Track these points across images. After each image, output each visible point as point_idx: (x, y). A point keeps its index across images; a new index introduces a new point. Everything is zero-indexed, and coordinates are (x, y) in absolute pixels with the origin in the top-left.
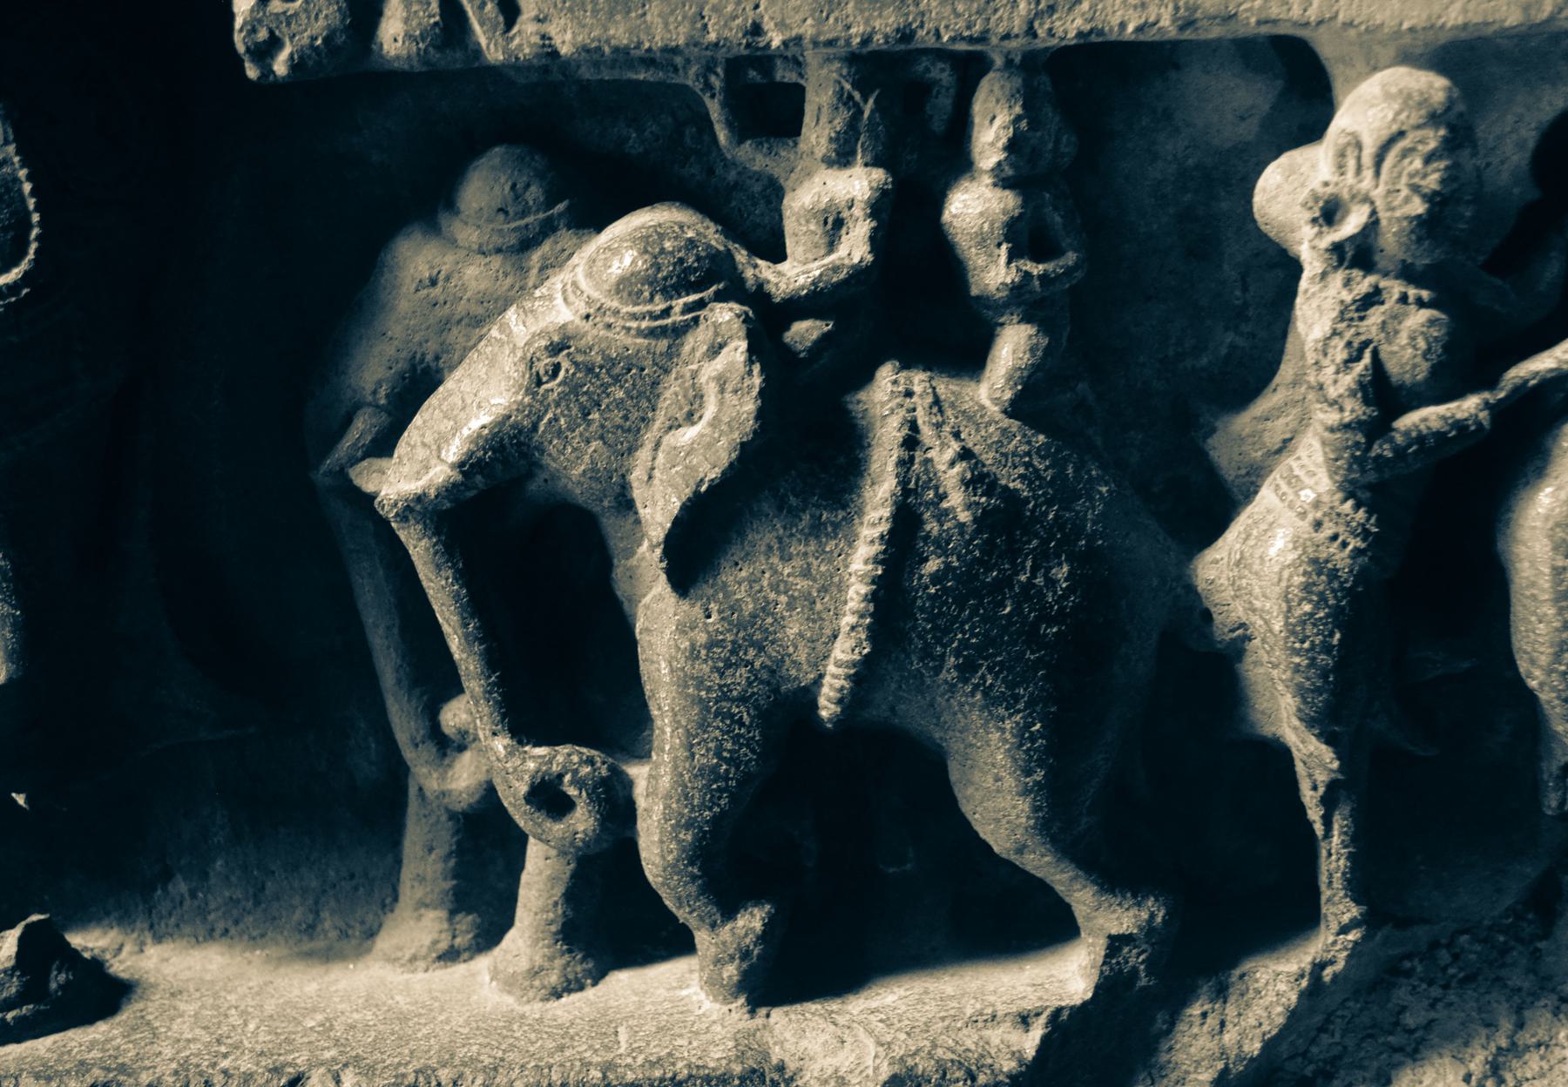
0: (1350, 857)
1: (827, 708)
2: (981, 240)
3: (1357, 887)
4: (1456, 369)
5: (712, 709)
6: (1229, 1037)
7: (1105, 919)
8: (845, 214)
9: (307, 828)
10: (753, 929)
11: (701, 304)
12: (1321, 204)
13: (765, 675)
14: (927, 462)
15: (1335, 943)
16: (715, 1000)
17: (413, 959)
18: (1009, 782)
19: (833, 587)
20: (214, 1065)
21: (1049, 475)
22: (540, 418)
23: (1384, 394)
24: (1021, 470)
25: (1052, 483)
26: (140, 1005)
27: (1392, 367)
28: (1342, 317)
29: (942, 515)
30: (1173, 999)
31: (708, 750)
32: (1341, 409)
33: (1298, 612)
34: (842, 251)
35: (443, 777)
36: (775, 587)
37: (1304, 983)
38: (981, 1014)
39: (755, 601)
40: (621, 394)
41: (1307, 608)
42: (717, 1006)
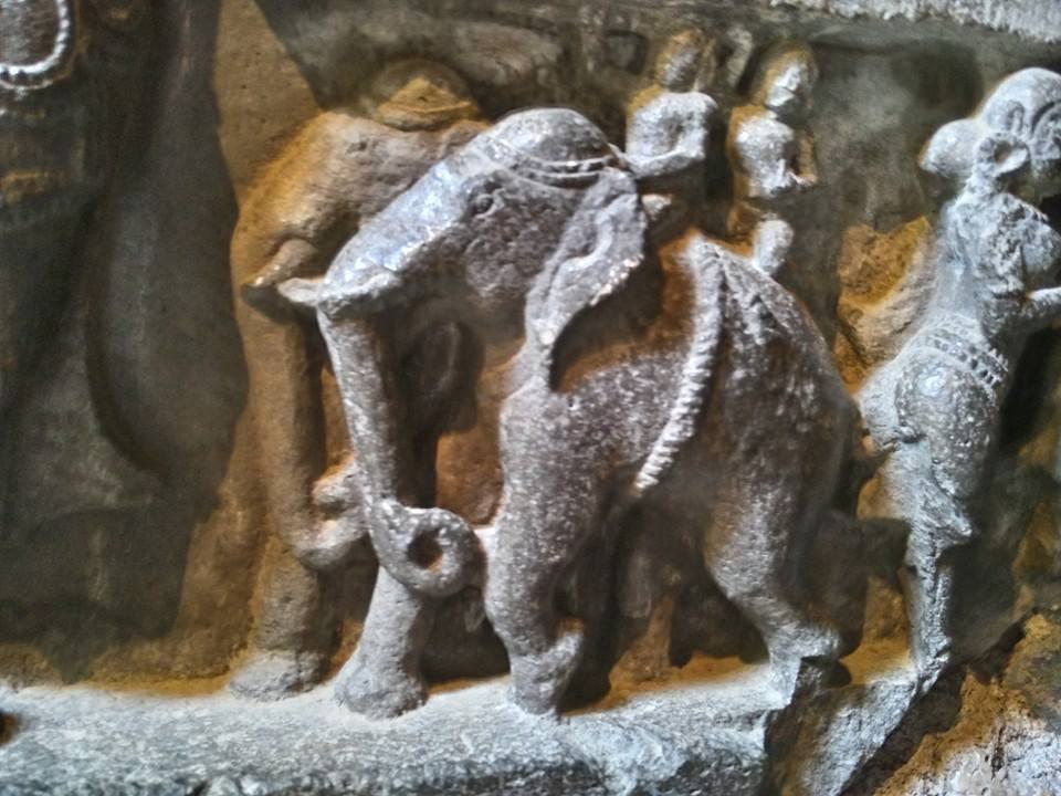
0: (947, 603)
1: (646, 478)
2: (767, 156)
5: (561, 477)
6: (864, 735)
7: (798, 646)
8: (684, 124)
9: (133, 603)
10: (568, 653)
12: (995, 147)
13: (606, 453)
15: (933, 663)
16: (530, 711)
17: (268, 689)
18: (762, 540)
19: (669, 387)
20: (121, 779)
22: (470, 242)
26: (28, 734)
27: (1030, 261)
28: (1003, 223)
29: (747, 339)
30: (828, 706)
31: (559, 509)
32: (1007, 283)
33: (964, 422)
34: (680, 149)
35: (313, 539)
36: (625, 386)
37: (914, 692)
38: (721, 717)
39: (609, 395)
40: (535, 228)
41: (971, 419)
42: (532, 716)
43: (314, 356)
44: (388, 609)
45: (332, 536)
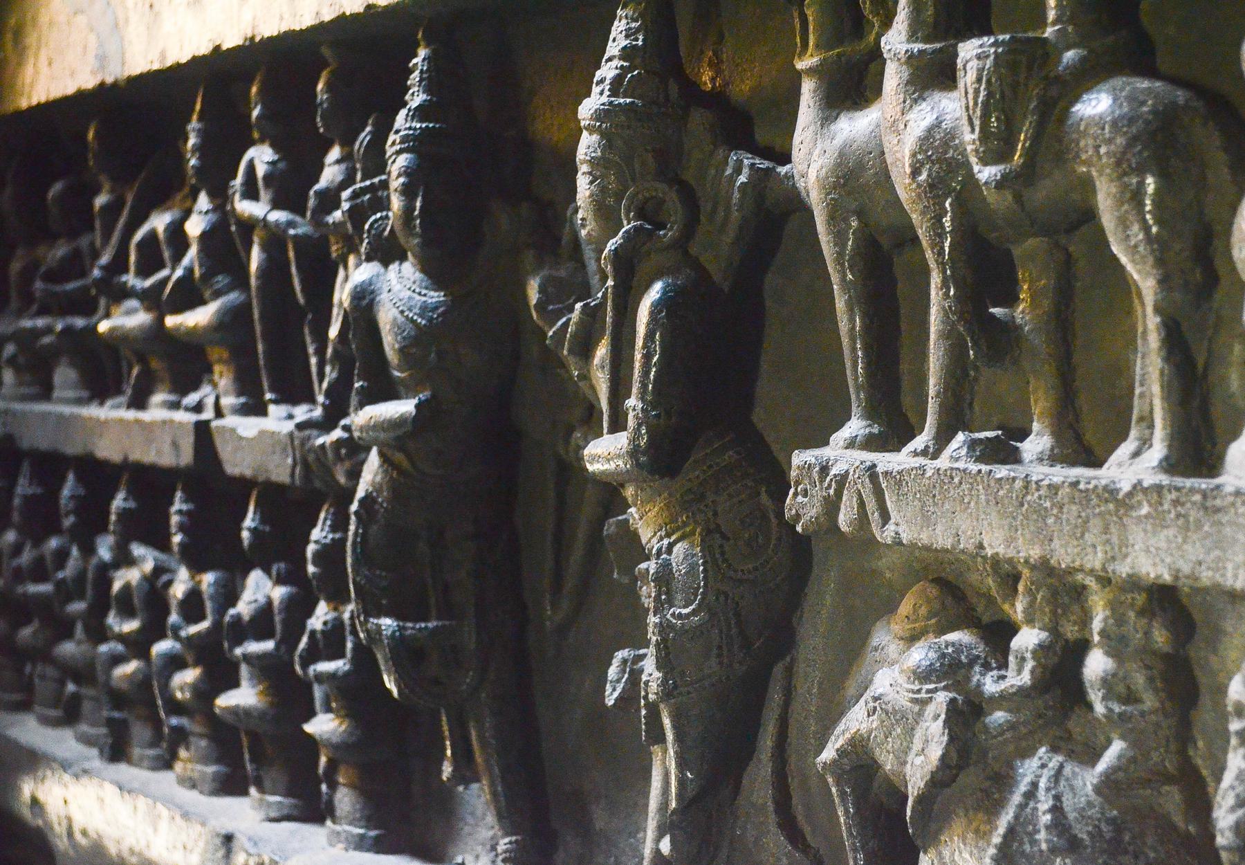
11: (935, 690)
14: (1036, 809)
21: (1108, 836)
24: (1090, 828)
25: (1109, 842)
29: (1034, 842)
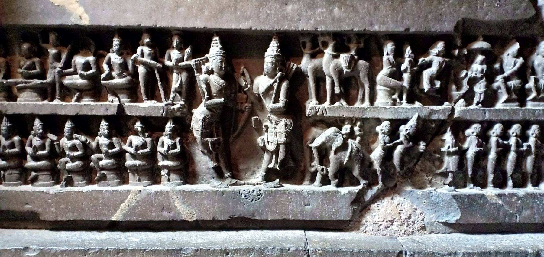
1: (344, 163)
3: (382, 181)
4: (390, 141)
7: (363, 182)
19: (346, 154)
23: (385, 143)
43: (312, 151)
44: (319, 177)
45: (313, 169)
